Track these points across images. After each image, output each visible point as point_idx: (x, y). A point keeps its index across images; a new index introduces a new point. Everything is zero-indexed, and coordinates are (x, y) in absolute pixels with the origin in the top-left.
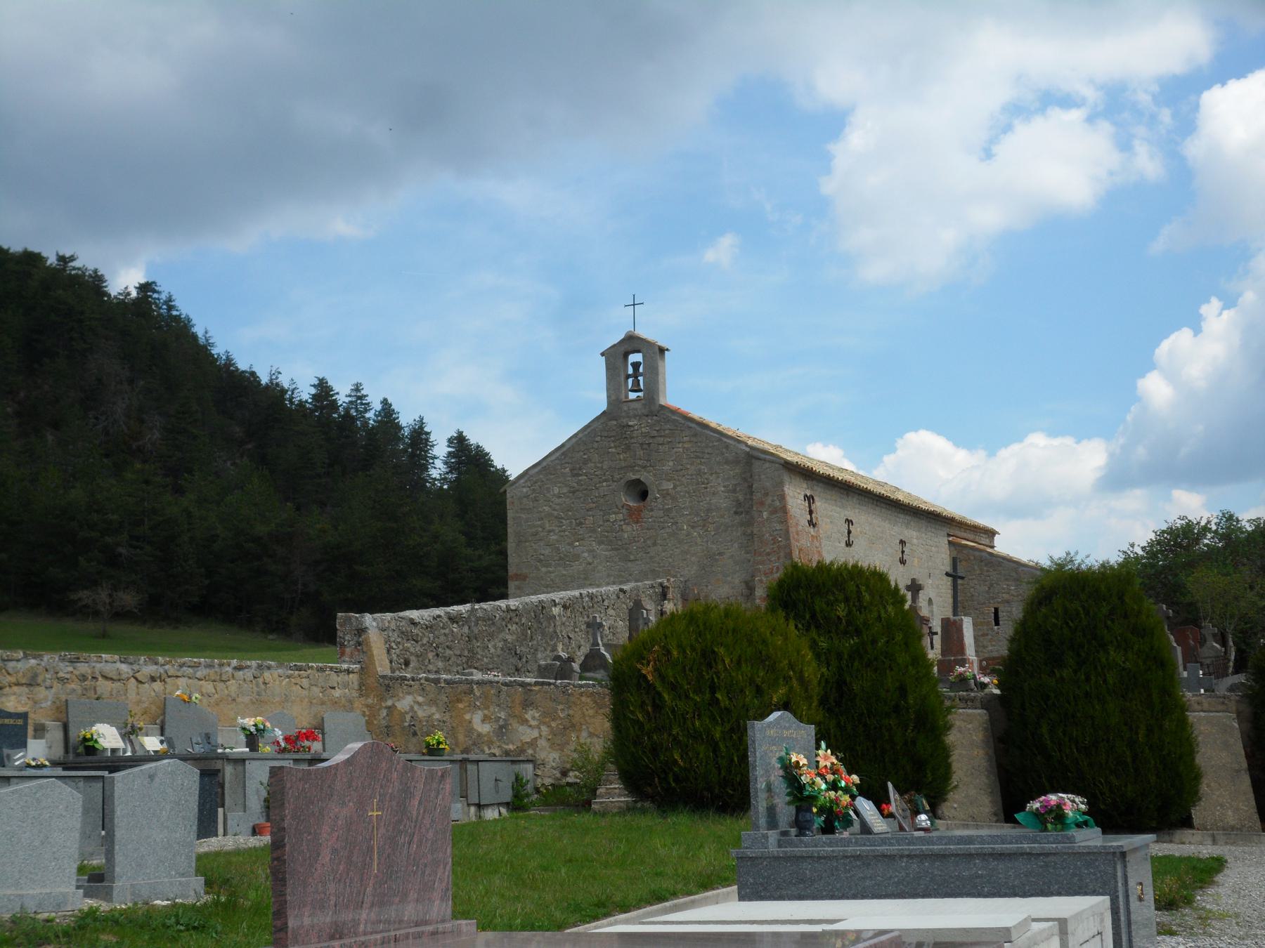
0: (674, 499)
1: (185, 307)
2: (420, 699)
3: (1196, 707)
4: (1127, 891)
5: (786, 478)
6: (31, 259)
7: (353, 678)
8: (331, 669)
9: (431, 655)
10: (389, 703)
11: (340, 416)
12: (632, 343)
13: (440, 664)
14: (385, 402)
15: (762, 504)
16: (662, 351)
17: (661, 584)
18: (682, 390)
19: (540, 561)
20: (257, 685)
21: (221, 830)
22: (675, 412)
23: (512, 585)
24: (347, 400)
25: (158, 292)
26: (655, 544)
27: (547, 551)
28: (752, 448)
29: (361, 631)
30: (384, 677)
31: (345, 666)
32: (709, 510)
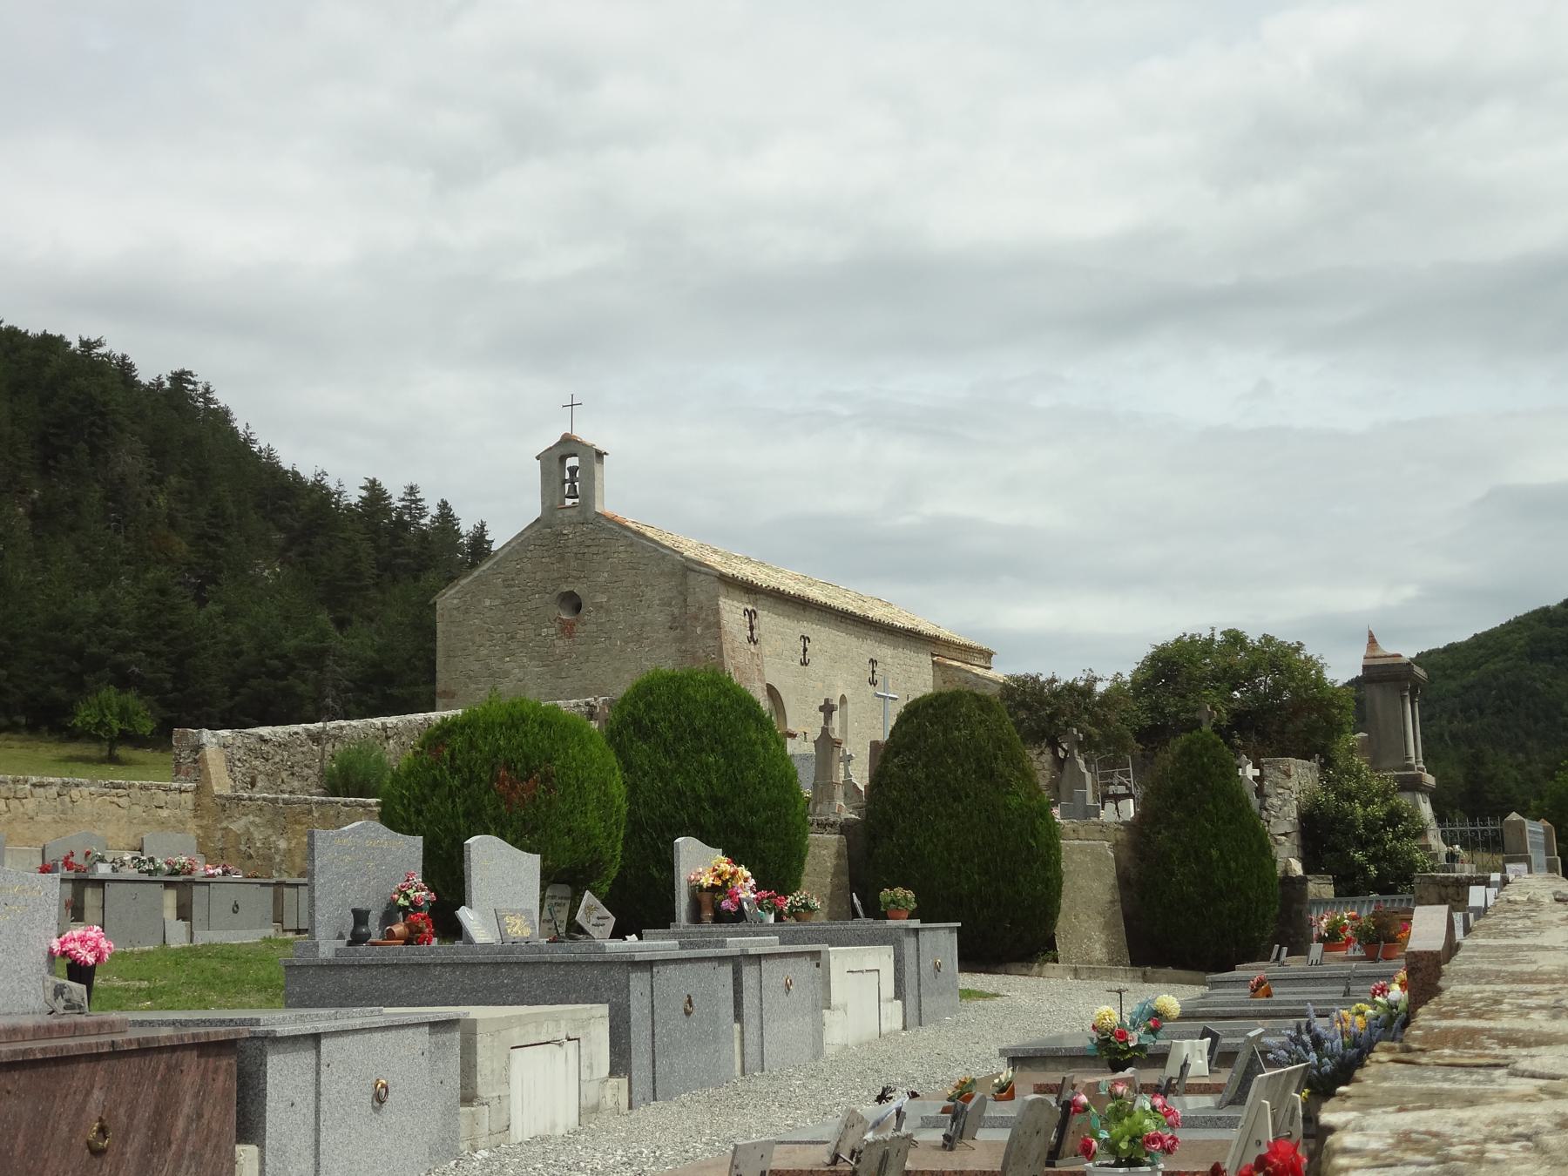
0: (608, 612)
1: (223, 397)
2: (257, 820)
3: (1072, 835)
4: (371, 1030)
5: (722, 589)
6: (51, 344)
7: (189, 797)
8: (158, 787)
9: (284, 775)
10: (224, 824)
11: (391, 522)
12: (569, 445)
13: (296, 784)
14: (444, 505)
15: (696, 618)
16: (600, 455)
17: (587, 704)
18: (619, 496)
19: (470, 678)
20: (62, 803)
21: (1274, 956)
22: (611, 520)
23: (440, 702)
24: (399, 504)
25: (195, 383)
26: (587, 660)
27: (476, 667)
28: (687, 559)
29: (198, 748)
30: (220, 796)
31: (176, 785)
32: (643, 625)
